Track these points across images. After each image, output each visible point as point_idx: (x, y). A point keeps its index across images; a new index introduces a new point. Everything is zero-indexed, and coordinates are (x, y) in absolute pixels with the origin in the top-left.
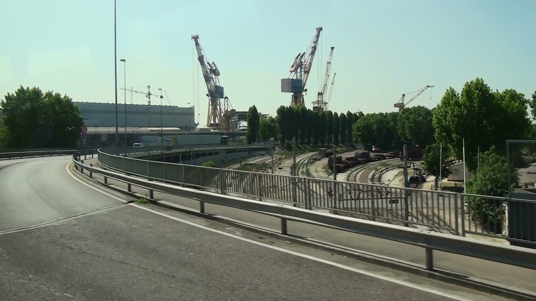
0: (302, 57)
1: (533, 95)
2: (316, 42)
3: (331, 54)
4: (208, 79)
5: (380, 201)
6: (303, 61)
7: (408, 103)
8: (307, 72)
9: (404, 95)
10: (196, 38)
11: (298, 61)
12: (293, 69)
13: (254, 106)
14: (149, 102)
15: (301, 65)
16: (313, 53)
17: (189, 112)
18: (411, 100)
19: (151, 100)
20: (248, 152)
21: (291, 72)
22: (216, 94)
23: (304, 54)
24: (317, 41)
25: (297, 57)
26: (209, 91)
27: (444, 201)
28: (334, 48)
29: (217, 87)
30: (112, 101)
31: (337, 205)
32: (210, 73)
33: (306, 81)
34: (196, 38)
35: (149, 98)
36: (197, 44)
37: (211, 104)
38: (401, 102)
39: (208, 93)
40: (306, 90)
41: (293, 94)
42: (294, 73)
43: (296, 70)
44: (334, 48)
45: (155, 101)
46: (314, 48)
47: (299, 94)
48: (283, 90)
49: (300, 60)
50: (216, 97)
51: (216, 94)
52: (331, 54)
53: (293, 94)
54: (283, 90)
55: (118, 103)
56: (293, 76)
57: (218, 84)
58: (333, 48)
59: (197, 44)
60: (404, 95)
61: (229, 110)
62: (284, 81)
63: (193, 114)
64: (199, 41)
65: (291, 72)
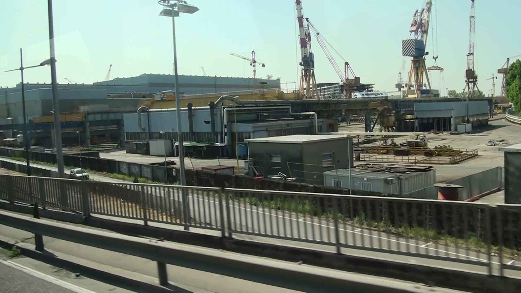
1: (127, 152)
5: (254, 207)
8: (425, 32)
9: (508, 59)
12: (414, 28)
13: (278, 80)
14: (254, 71)
15: (421, 26)
16: (429, 10)
20: (209, 119)
22: (308, 62)
23: (423, 10)
26: (303, 59)
30: (172, 73)
31: (158, 191)
32: (42, 64)
35: (254, 66)
39: (301, 61)
40: (427, 53)
41: (412, 58)
42: (413, 33)
48: (404, 54)
51: (308, 62)
54: (404, 54)
55: (179, 74)
56: (413, 37)
61: (351, 77)
62: (406, 44)
65: (411, 32)
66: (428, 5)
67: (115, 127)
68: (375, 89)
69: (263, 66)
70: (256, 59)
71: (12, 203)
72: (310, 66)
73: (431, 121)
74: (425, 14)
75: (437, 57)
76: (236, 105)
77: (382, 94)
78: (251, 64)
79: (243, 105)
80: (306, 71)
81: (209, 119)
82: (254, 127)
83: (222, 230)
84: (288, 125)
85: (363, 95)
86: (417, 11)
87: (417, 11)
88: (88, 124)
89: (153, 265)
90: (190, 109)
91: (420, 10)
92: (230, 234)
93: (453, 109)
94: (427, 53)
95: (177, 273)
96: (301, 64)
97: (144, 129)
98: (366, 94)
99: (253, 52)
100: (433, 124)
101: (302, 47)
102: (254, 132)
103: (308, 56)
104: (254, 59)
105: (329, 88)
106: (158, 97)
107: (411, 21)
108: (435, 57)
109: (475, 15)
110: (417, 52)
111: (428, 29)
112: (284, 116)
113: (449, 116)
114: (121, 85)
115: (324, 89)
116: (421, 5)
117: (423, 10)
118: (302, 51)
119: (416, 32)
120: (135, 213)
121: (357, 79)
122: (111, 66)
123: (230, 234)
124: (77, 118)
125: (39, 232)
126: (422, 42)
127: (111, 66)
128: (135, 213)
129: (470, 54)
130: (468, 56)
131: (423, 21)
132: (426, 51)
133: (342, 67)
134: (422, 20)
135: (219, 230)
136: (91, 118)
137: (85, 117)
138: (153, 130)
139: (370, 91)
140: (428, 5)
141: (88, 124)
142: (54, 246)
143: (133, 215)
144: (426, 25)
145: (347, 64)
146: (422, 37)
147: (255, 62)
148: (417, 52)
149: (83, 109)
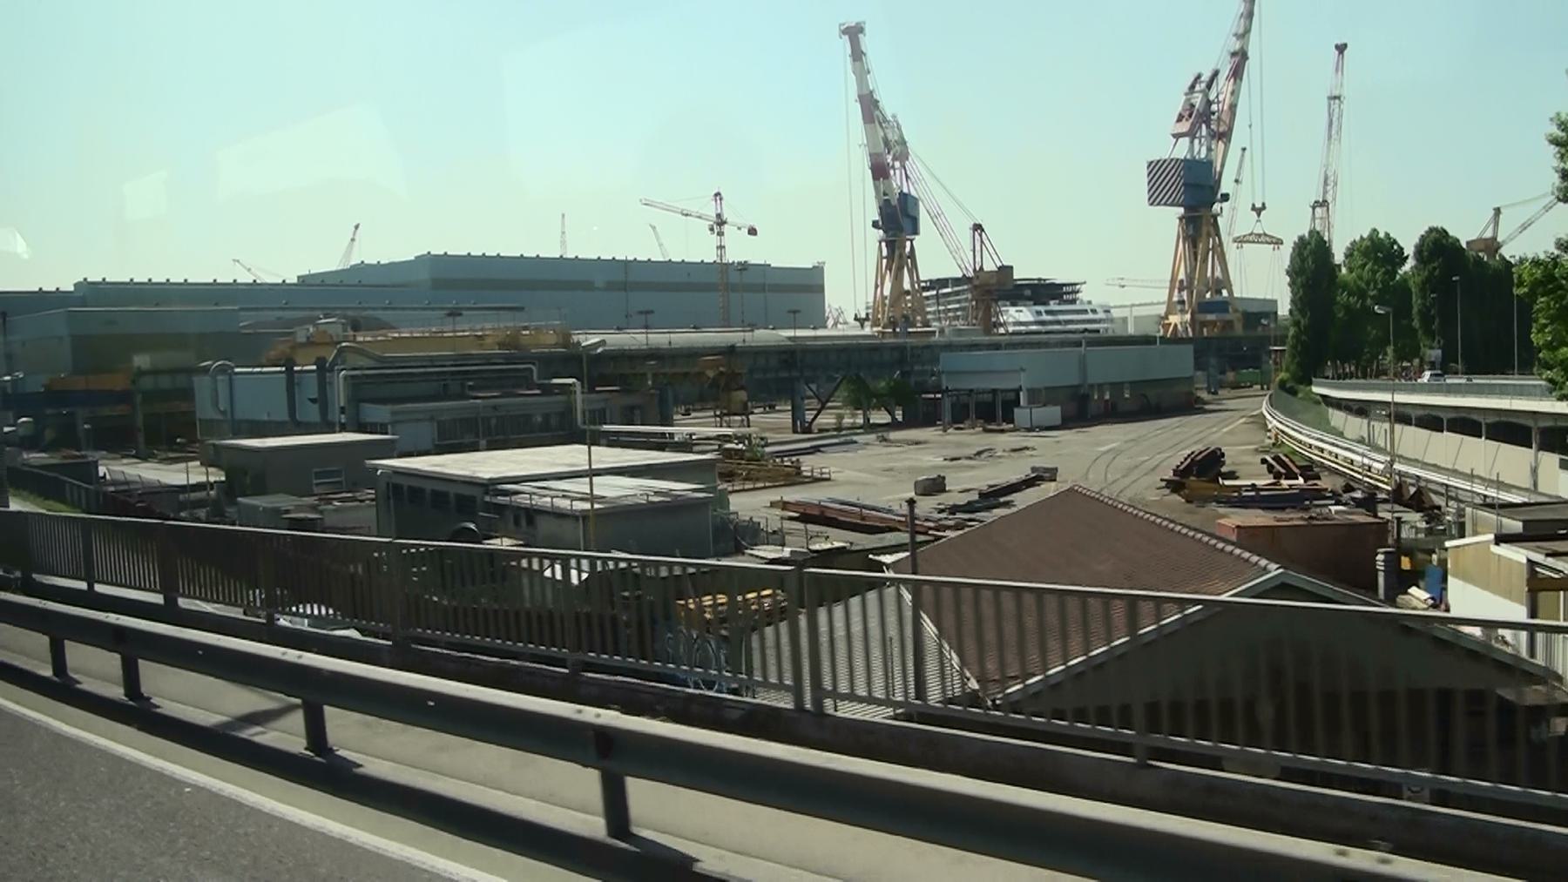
0: (1209, 86)
2: (1244, 35)
3: (1339, 68)
4: (880, 171)
6: (1212, 97)
7: (1511, 238)
8: (1225, 136)
9: (1498, 211)
10: (853, 33)
11: (1198, 100)
12: (1185, 126)
13: (818, 271)
14: (721, 247)
15: (1206, 117)
16: (1237, 73)
17: (803, 288)
18: (1524, 227)
19: (726, 241)
21: (1177, 136)
22: (898, 219)
23: (1216, 74)
24: (1247, 31)
25: (1192, 87)
27: (544, 595)
28: (1345, 46)
29: (904, 197)
33: (1223, 166)
34: (853, 33)
35: (721, 234)
36: (857, 55)
37: (885, 253)
38: (1488, 234)
40: (1225, 197)
41: (1181, 210)
43: (1192, 134)
44: (1345, 46)
45: (740, 250)
46: (1241, 57)
47: (1202, 212)
48: (1154, 201)
49: (1206, 95)
50: (901, 230)
52: (1339, 68)
53: (1181, 210)
54: (1154, 201)
56: (1182, 150)
57: (905, 190)
58: (1341, 49)
59: (857, 55)
60: (1498, 211)
61: (989, 266)
63: (819, 289)
64: (866, 42)
65: (1177, 136)
66: (1237, 59)
67: (121, 410)
68: (1084, 295)
69: (753, 232)
70: (725, 217)
71: (171, 601)
72: (901, 230)
73: (988, 397)
74: (1223, 86)
75: (1264, 207)
76: (372, 363)
77: (1094, 311)
78: (712, 229)
79: (384, 362)
80: (891, 245)
81: (315, 396)
82: (394, 413)
83: (797, 691)
84: (495, 408)
85: (1039, 313)
86: (1199, 77)
87: (1199, 77)
88: (139, 398)
89: (585, 782)
90: (290, 371)
91: (1206, 77)
92: (818, 703)
93: (1023, 370)
94: (1225, 197)
95: (661, 811)
96: (875, 225)
97: (223, 413)
98: (1048, 312)
99: (718, 194)
100: (992, 405)
101: (875, 178)
102: (394, 423)
103: (894, 202)
104: (719, 216)
105: (957, 293)
106: (301, 339)
107: (1178, 105)
108: (1259, 205)
109: (1345, 93)
110: (1193, 191)
111: (1231, 129)
112: (520, 386)
113: (1015, 386)
114: (360, 284)
115: (948, 295)
116: (1213, 56)
117: (1216, 74)
118: (877, 188)
119: (1192, 134)
120: (878, 673)
121: (1006, 270)
122: (357, 227)
123: (818, 703)
124: (118, 383)
125: (317, 693)
126: (1209, 164)
127: (357, 227)
128: (878, 673)
129: (1316, 205)
130: (1314, 208)
131: (1214, 107)
132: (1224, 189)
133: (965, 236)
134: (1209, 103)
135: (787, 688)
136: (147, 383)
137: (134, 382)
138: (239, 415)
139: (1073, 302)
140: (1237, 59)
141: (139, 398)
142: (350, 733)
143: (780, 678)
144: (1225, 117)
145: (978, 228)
146: (1209, 149)
147: (721, 222)
148: (1193, 191)
149: (142, 361)
